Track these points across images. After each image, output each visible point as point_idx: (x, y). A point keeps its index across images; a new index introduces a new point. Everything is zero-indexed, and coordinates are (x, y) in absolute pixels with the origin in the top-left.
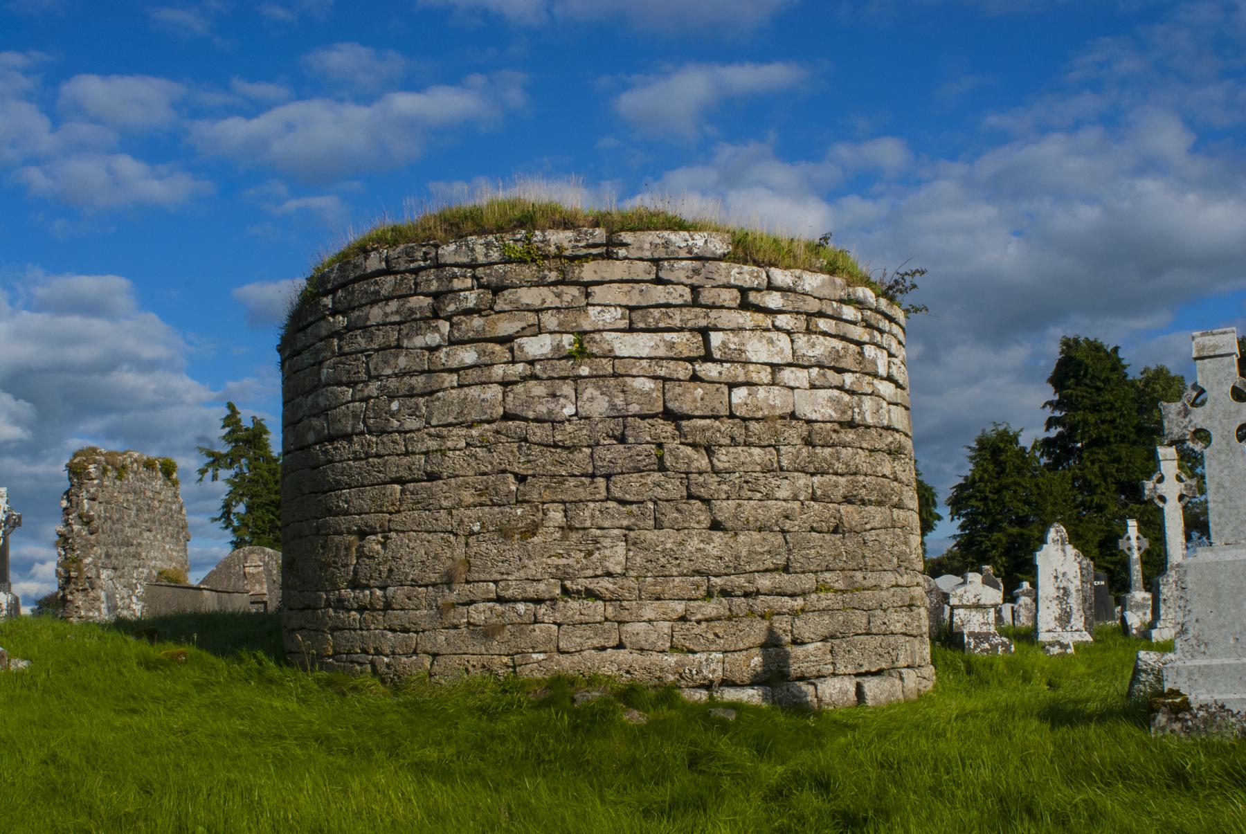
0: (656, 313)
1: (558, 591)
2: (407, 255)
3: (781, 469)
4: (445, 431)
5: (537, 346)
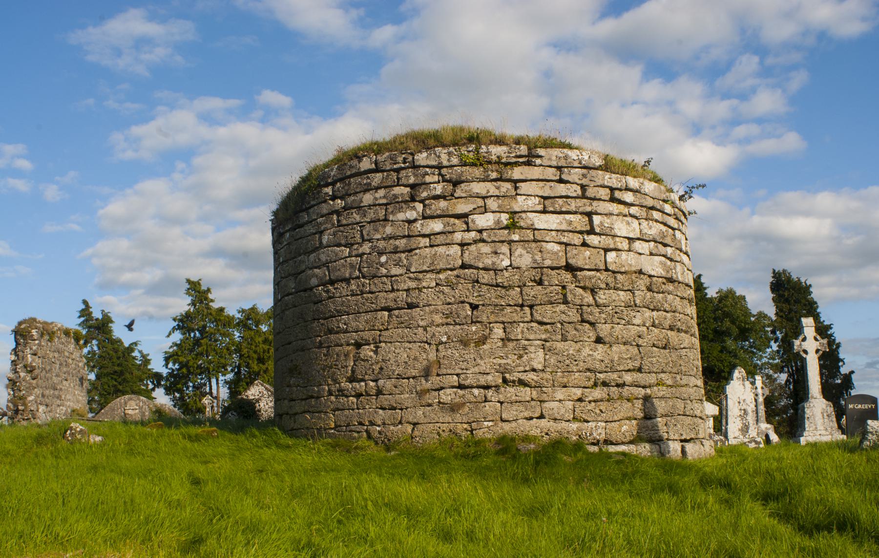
0: (560, 201)
1: (501, 381)
2: (391, 159)
3: (636, 305)
4: (421, 276)
5: (483, 221)
